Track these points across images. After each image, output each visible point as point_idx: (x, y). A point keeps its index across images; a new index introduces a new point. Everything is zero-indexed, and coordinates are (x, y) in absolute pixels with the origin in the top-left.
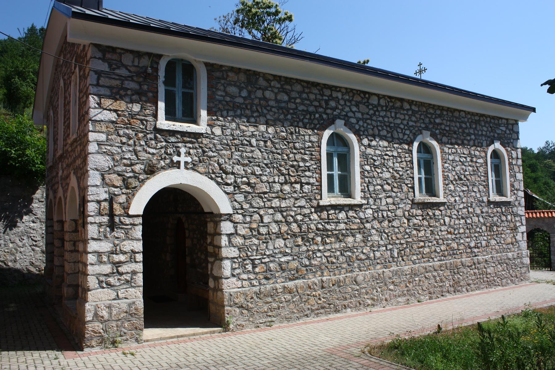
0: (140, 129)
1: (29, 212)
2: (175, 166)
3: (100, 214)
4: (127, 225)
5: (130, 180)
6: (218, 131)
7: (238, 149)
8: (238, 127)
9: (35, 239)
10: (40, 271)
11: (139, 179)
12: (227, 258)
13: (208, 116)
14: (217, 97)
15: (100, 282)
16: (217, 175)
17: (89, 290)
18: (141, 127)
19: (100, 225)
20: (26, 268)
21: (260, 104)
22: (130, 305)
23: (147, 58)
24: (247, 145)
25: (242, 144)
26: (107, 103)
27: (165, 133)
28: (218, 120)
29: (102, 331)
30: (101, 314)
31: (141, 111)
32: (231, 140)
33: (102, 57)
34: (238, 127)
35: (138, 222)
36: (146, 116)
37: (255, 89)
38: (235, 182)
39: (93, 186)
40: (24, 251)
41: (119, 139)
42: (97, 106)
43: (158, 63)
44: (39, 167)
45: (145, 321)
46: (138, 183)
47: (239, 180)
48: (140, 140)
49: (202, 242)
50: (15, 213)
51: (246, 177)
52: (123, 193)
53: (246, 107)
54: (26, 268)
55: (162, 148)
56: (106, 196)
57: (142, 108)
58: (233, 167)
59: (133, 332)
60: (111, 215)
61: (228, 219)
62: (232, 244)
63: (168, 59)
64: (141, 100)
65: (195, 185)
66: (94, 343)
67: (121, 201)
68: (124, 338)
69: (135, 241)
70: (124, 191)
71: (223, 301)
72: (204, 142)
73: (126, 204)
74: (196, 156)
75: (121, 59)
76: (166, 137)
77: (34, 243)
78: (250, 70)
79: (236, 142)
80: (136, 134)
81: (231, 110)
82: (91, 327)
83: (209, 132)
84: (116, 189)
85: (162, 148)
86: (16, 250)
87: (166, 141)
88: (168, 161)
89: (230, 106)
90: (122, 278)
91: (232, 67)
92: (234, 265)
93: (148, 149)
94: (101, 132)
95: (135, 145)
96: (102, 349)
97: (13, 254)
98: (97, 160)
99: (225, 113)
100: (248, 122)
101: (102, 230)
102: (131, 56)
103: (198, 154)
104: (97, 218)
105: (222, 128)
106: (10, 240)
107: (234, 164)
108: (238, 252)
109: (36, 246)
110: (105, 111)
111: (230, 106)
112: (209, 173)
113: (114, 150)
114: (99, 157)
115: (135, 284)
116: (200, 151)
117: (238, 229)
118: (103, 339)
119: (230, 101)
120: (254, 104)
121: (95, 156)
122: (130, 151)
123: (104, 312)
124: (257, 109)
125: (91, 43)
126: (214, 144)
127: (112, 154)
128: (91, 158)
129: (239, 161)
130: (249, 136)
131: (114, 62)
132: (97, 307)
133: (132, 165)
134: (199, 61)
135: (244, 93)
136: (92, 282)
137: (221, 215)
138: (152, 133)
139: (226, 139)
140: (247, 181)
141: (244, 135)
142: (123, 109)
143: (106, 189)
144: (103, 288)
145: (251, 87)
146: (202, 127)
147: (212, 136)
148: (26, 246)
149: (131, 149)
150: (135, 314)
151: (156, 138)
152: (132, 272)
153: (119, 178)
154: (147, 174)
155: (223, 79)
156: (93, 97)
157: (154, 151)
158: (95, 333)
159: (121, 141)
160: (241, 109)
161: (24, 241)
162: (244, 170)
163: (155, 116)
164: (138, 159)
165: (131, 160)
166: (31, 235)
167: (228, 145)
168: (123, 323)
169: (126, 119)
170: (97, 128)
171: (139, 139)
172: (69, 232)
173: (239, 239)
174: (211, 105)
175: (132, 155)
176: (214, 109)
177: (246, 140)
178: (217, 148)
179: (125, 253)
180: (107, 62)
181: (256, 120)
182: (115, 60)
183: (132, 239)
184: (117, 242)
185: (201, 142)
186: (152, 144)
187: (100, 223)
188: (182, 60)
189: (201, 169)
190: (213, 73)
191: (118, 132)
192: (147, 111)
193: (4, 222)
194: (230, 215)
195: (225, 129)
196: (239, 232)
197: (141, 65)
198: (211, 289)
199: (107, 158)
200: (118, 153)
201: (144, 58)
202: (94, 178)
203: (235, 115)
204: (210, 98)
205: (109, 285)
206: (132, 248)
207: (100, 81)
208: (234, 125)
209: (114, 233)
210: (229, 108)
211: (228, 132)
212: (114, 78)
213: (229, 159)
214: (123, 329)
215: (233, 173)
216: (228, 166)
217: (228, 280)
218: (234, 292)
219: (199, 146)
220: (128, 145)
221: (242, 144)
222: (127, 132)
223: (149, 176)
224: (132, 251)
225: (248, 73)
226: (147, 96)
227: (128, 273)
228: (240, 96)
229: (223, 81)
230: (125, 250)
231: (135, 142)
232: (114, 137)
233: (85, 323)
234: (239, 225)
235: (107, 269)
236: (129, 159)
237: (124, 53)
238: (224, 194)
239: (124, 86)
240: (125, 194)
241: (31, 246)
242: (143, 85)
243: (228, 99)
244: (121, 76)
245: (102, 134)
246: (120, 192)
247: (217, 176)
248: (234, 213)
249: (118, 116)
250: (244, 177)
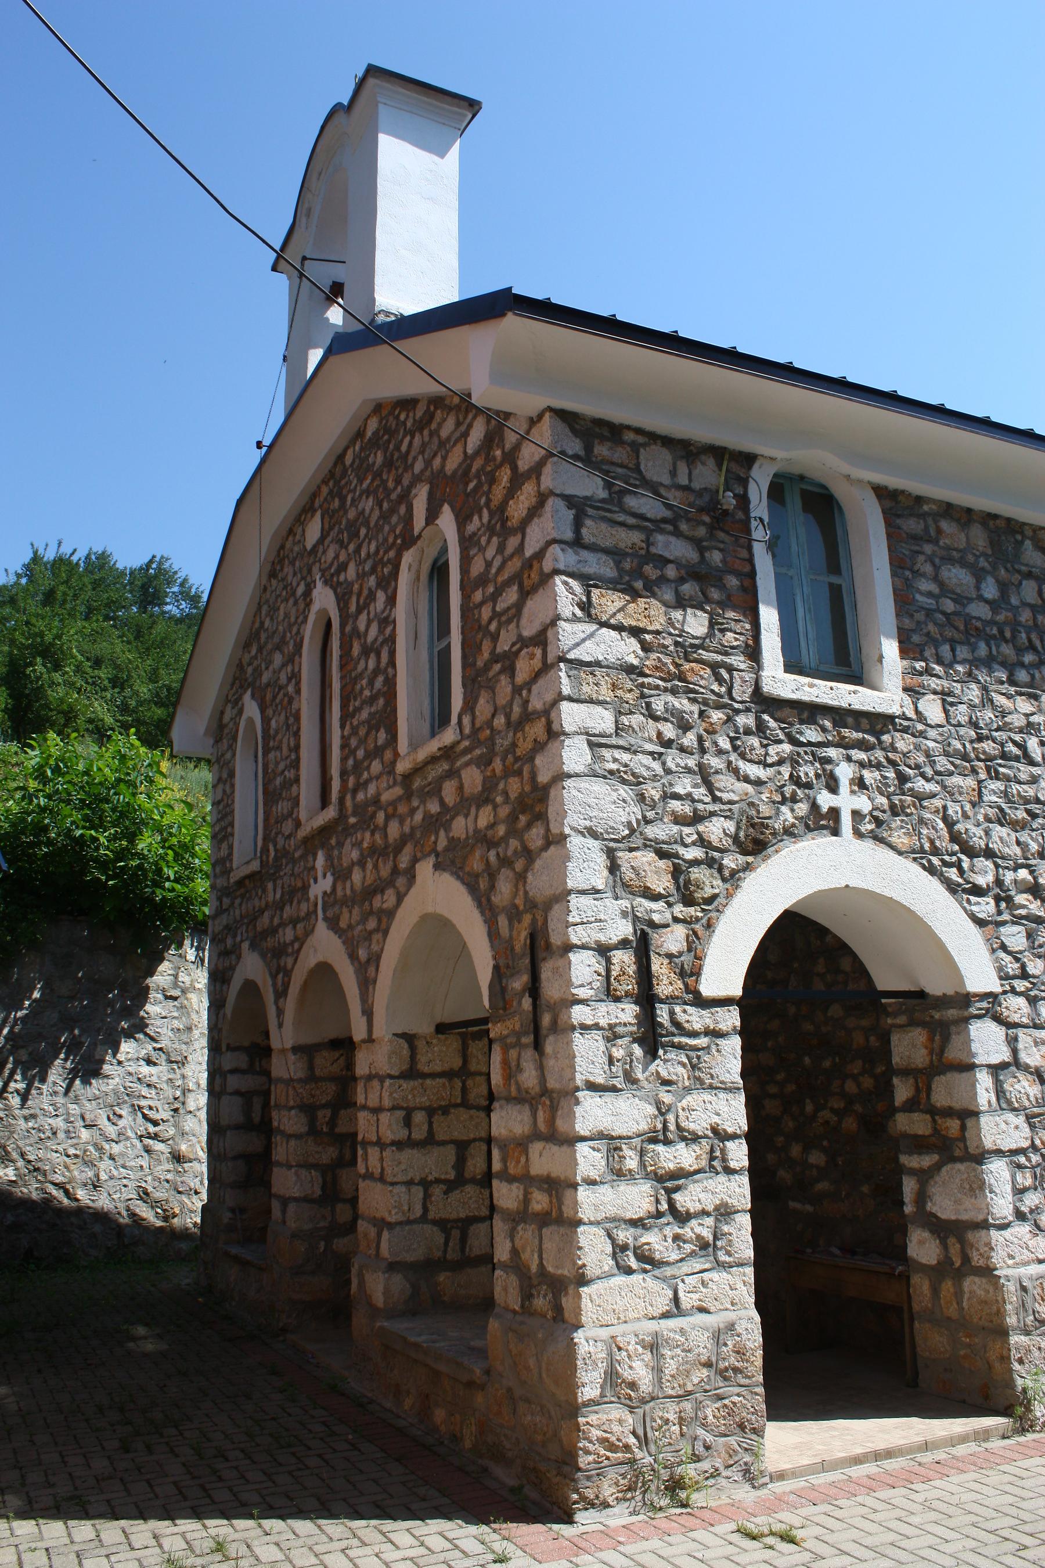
0: (713, 697)
1: (139, 1027)
2: (824, 827)
3: (611, 994)
4: (694, 1034)
5: (697, 874)
6: (932, 709)
7: (997, 772)
8: (987, 701)
9: (152, 1114)
10: (166, 1219)
11: (720, 870)
12: (999, 1152)
13: (902, 658)
14: (918, 597)
15: (619, 1249)
16: (947, 858)
17: (583, 1280)
18: (715, 687)
19: (612, 1035)
20: (128, 1209)
21: (1036, 625)
22: (718, 1336)
23: (711, 462)
24: (1017, 759)
25: (1004, 756)
26: (609, 602)
27: (787, 711)
28: (928, 672)
29: (632, 1440)
30: (627, 1374)
31: (710, 634)
32: (972, 742)
33: (582, 453)
34: (987, 701)
35: (730, 1023)
36: (726, 654)
37: (1018, 577)
38: (999, 882)
39: (583, 892)
40: (122, 1155)
41: (652, 727)
42: (579, 613)
43: (744, 482)
44: (173, 890)
45: (768, 1402)
46: (720, 882)
47: (1009, 877)
48: (714, 732)
49: (809, 1108)
50: (98, 1031)
51: (1027, 866)
52: (676, 920)
53: (1001, 632)
54: (128, 1209)
55: (780, 762)
56: (624, 929)
57: (712, 625)
58: (987, 832)
59: (732, 1440)
60: (646, 998)
61: (987, 1010)
62: (1009, 1102)
63: (771, 470)
64: (708, 600)
65: (887, 893)
66: (608, 1491)
67: (674, 949)
68: (705, 1465)
69: (722, 1095)
70: (679, 910)
71: (1000, 1313)
72: (900, 745)
73: (687, 959)
74: (882, 794)
75: (638, 465)
76: (791, 724)
77: (152, 1129)
78: (995, 517)
79: (988, 746)
80: (702, 713)
81: (961, 643)
82: (598, 1427)
83: (911, 714)
84: (654, 906)
85: (780, 762)
86: (100, 1149)
87: (794, 741)
88: (802, 808)
89: (957, 629)
90: (687, 1232)
91: (949, 506)
92: (1019, 1178)
93: (742, 764)
94: (599, 703)
95: (703, 751)
96: (634, 1513)
97: (90, 1164)
98: (590, 802)
99: (945, 650)
100: (1012, 682)
101: (618, 1053)
102: (664, 456)
103: (887, 785)
104: (603, 1008)
105: (944, 701)
106: (83, 1118)
107: (990, 821)
108: (1026, 1131)
109: (155, 1137)
110: (604, 630)
111: (957, 629)
112: (922, 850)
113: (642, 764)
114: (598, 787)
115: (729, 1253)
116: (891, 774)
117: (1020, 1046)
118: (639, 1474)
119: (955, 613)
120: (1019, 624)
121: (584, 784)
122: (689, 770)
123: (637, 1364)
124: (1030, 640)
125: (550, 409)
126: (928, 755)
127: (637, 781)
128: (574, 792)
129: (1001, 810)
130: (1021, 731)
131: (620, 470)
132: (614, 1346)
133: (697, 818)
134: (860, 481)
135: (990, 590)
136: (593, 1249)
137: (966, 999)
138: (748, 710)
139: (960, 738)
140: (1030, 878)
141: (1006, 724)
142: (659, 627)
143: (624, 904)
144: (629, 1271)
145: (1007, 569)
146: (886, 696)
147: (920, 727)
148: (128, 1138)
149: (691, 762)
150: (736, 1370)
151: (761, 728)
152: (717, 1208)
153: (662, 864)
154: (745, 853)
155: (929, 541)
156: (565, 583)
157: (754, 771)
158: (612, 1448)
159: (659, 734)
160: (988, 639)
161: (121, 1123)
162: (1018, 843)
163: (754, 653)
164: (716, 799)
165: (693, 801)
166: (143, 1103)
167: (965, 757)
168: (698, 1406)
169: (667, 660)
170: (586, 689)
171: (711, 732)
172: (391, 1077)
173: (1025, 1084)
174: (907, 623)
175: (696, 786)
176: (916, 638)
177: (1015, 743)
178: (939, 768)
179: (694, 1138)
180: (601, 470)
181: (1033, 677)
182: (621, 466)
183: (711, 1087)
184: (667, 1098)
185: (892, 744)
186: (752, 749)
187: (611, 1027)
188: (802, 478)
189: (900, 838)
190: (898, 521)
191: (648, 705)
192: (729, 635)
193: (66, 1060)
194: (992, 997)
195: (952, 704)
196: (1024, 1057)
197: (696, 485)
198: (924, 1268)
199: (622, 792)
200: (655, 778)
201: (704, 464)
202: (585, 865)
203: (976, 659)
204: (903, 601)
205: (648, 1260)
206: (716, 1119)
207: (584, 531)
208: (974, 693)
209: (657, 1066)
210: (957, 636)
211: (961, 713)
212: (622, 524)
213: (974, 805)
214: (700, 1432)
215: (989, 854)
216: (973, 829)
217: (1007, 1233)
218: (1030, 1278)
219: (887, 759)
220: (682, 749)
221: (1004, 756)
222: (677, 705)
223: (750, 859)
224: (715, 1130)
225: (991, 523)
226: (722, 587)
227: (705, 1213)
228: (981, 598)
229: (928, 549)
230: (692, 1126)
231: (700, 740)
232: (636, 720)
233: (573, 1409)
234: (1021, 1033)
235: (637, 1198)
236: (689, 796)
237: (644, 445)
238: (971, 925)
239: (653, 550)
240: (684, 921)
241: (140, 1137)
242: (708, 549)
243: (949, 606)
244: (642, 517)
245: (599, 709)
246: (669, 916)
247: (945, 864)
248: (1005, 992)
249: (643, 649)
250: (1022, 866)
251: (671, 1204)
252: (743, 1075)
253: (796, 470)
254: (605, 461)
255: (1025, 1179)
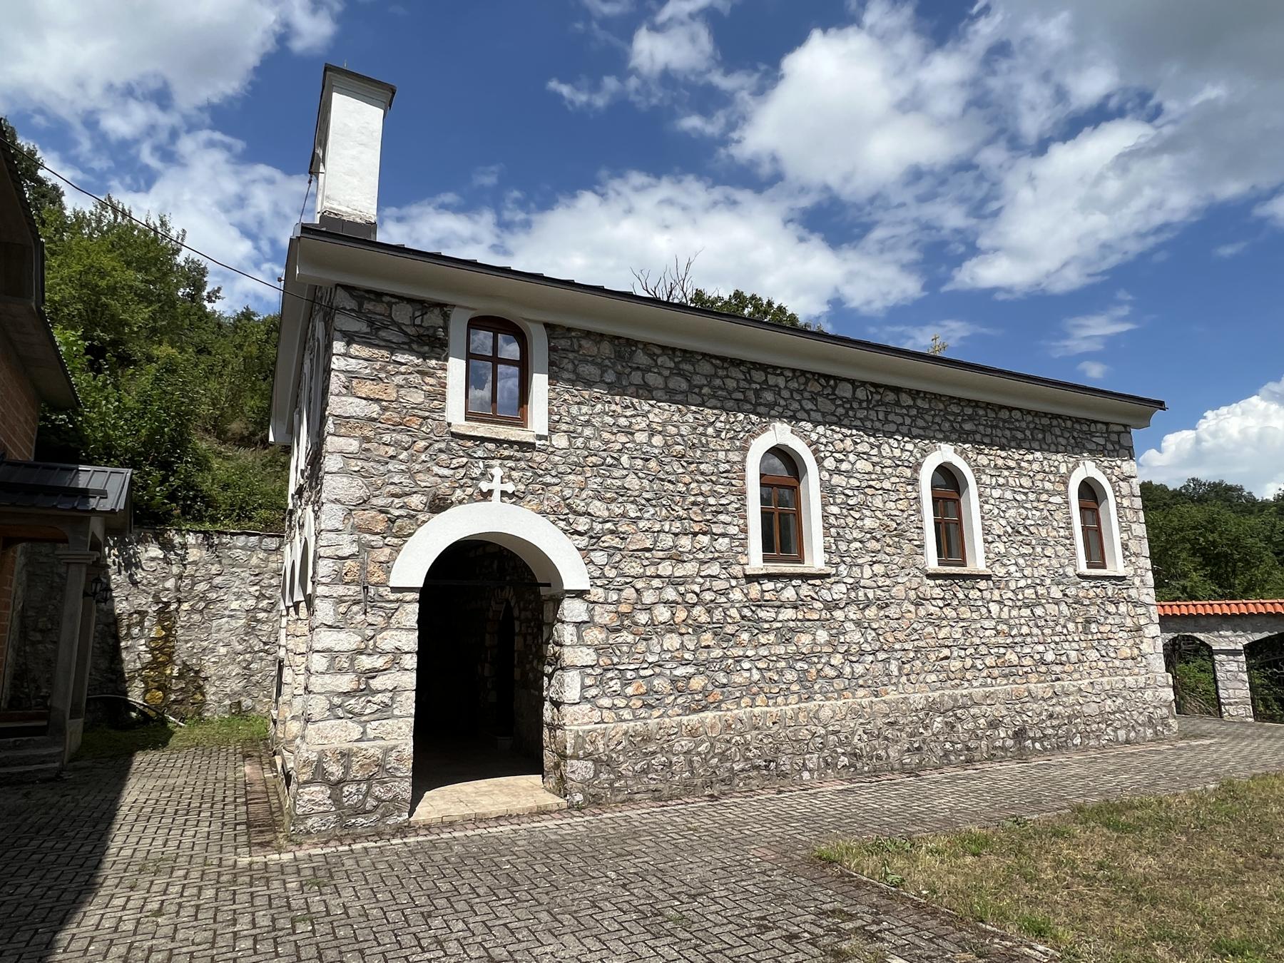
12: (575, 667)
84: (373, 538)
102: (408, 309)
229: (571, 356)
251: (367, 684)
252: (418, 622)
253: (1069, 143)
254: (370, 311)
255: (588, 681)
